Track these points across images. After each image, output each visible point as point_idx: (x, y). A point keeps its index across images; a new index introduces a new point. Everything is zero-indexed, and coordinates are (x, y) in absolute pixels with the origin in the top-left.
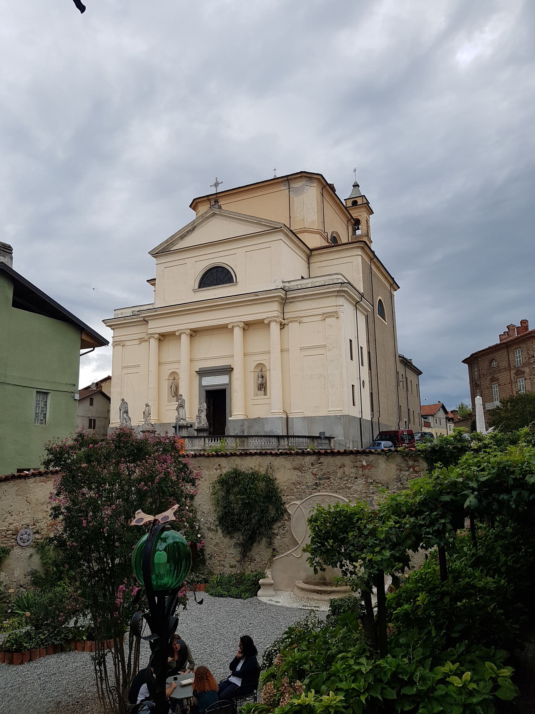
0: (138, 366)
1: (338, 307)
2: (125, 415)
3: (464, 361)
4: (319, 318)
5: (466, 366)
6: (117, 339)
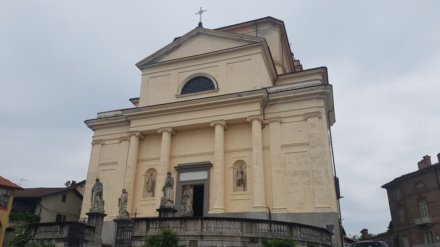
0: (116, 163)
1: (320, 108)
2: (98, 197)
3: (383, 187)
4: (301, 118)
5: (385, 190)
6: (96, 138)
